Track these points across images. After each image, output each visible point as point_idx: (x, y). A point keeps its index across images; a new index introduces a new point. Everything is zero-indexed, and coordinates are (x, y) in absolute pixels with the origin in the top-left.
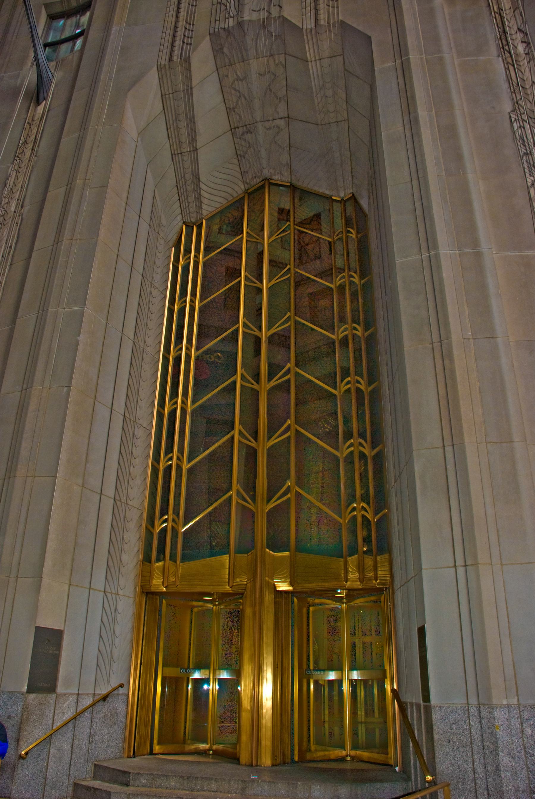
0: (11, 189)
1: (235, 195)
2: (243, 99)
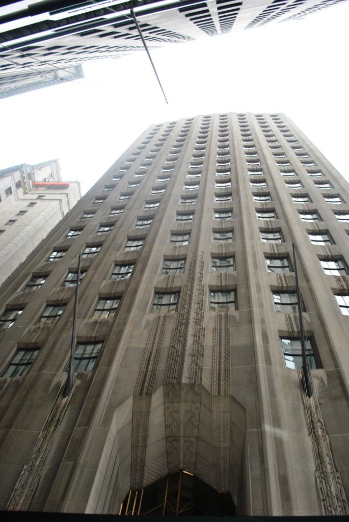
0: (39, 449)
1: (162, 475)
2: (175, 422)
